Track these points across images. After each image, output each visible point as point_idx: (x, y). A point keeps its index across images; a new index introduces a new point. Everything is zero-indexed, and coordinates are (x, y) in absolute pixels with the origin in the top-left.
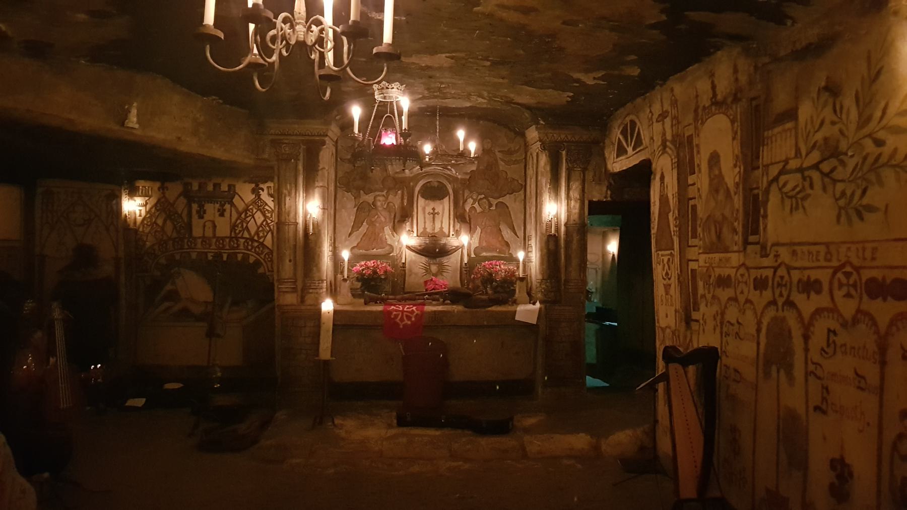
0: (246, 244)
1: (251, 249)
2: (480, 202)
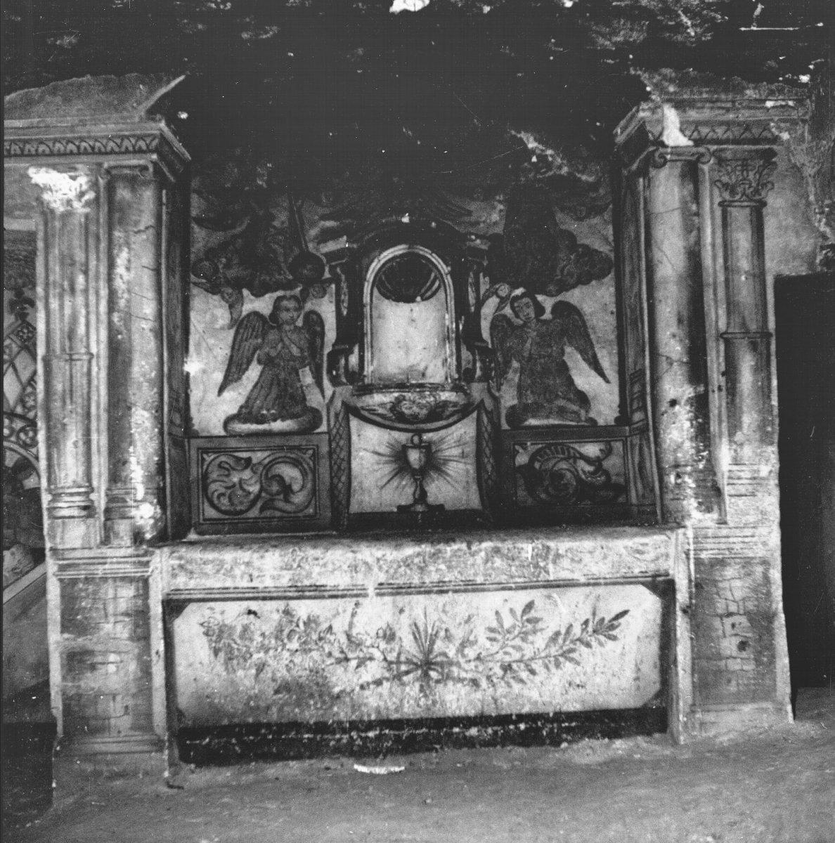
1: (10, 435)
2: (516, 305)
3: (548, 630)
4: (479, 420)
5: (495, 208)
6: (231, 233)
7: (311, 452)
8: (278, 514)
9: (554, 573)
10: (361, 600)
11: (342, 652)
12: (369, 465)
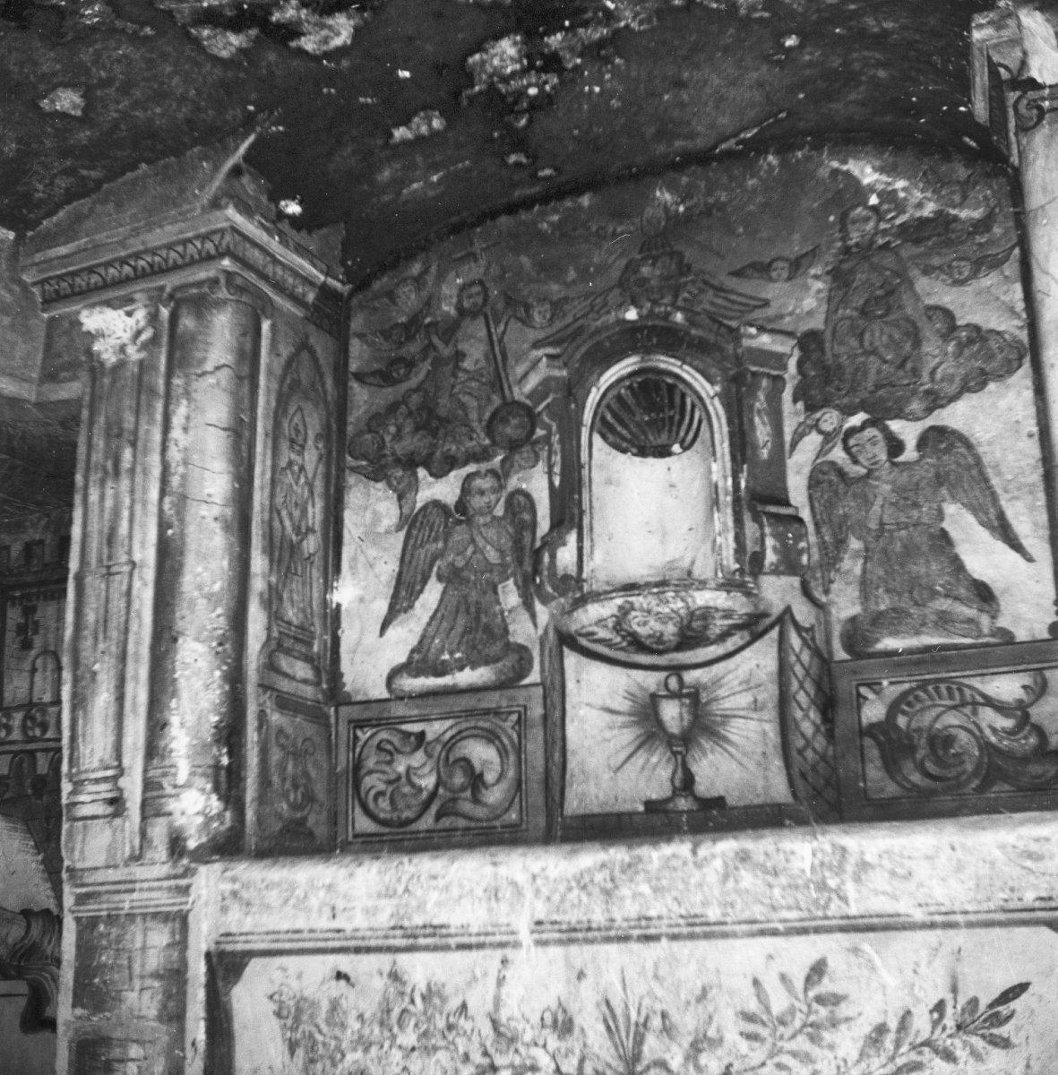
2: (852, 442)
3: (861, 1020)
4: (782, 641)
5: (808, 288)
6: (405, 386)
7: (514, 717)
8: (462, 823)
9: (861, 900)
10: (509, 952)
11: (486, 1054)
12: (595, 732)
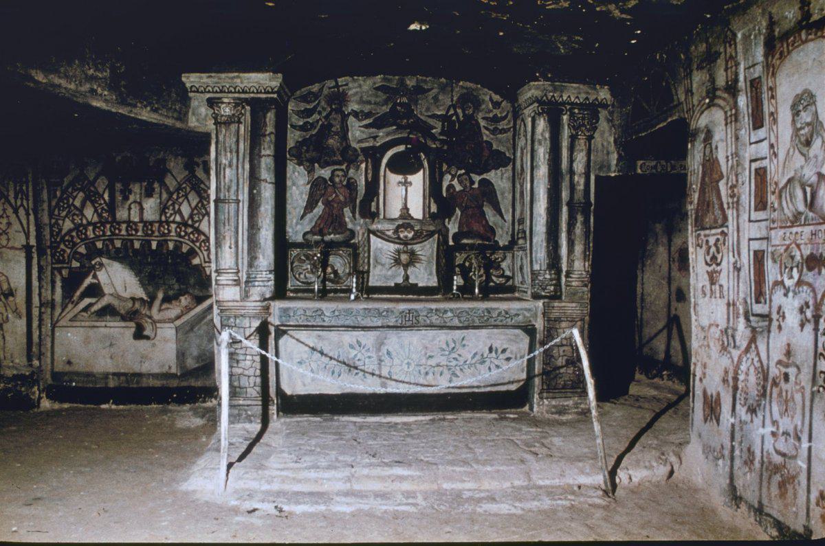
0: (178, 230)
